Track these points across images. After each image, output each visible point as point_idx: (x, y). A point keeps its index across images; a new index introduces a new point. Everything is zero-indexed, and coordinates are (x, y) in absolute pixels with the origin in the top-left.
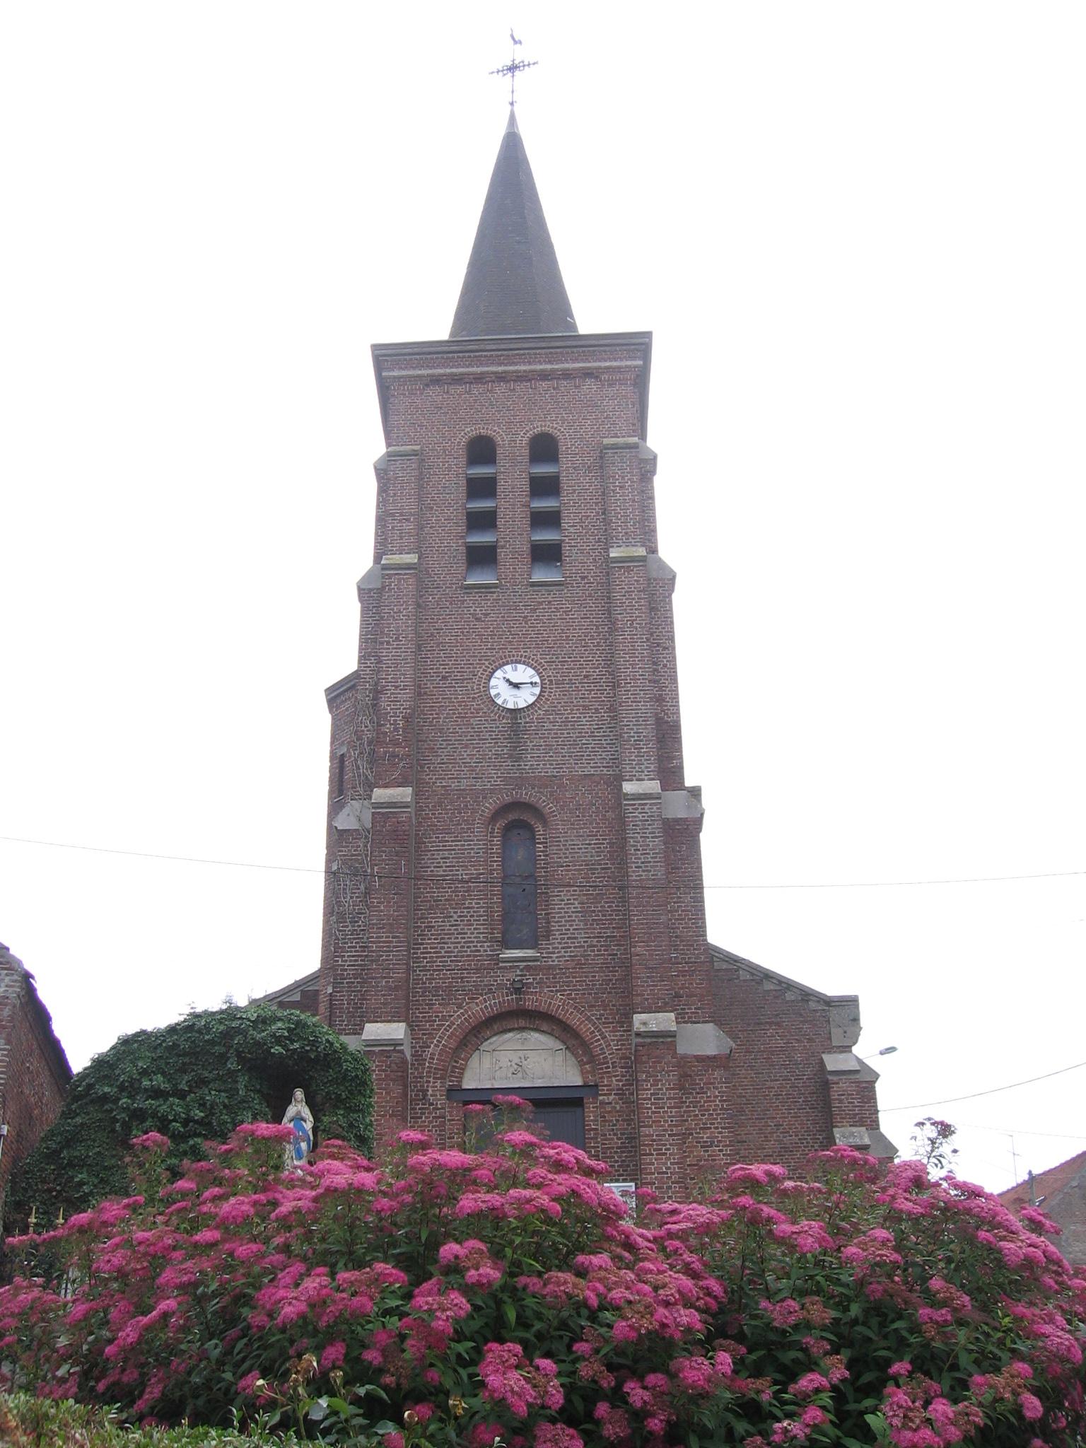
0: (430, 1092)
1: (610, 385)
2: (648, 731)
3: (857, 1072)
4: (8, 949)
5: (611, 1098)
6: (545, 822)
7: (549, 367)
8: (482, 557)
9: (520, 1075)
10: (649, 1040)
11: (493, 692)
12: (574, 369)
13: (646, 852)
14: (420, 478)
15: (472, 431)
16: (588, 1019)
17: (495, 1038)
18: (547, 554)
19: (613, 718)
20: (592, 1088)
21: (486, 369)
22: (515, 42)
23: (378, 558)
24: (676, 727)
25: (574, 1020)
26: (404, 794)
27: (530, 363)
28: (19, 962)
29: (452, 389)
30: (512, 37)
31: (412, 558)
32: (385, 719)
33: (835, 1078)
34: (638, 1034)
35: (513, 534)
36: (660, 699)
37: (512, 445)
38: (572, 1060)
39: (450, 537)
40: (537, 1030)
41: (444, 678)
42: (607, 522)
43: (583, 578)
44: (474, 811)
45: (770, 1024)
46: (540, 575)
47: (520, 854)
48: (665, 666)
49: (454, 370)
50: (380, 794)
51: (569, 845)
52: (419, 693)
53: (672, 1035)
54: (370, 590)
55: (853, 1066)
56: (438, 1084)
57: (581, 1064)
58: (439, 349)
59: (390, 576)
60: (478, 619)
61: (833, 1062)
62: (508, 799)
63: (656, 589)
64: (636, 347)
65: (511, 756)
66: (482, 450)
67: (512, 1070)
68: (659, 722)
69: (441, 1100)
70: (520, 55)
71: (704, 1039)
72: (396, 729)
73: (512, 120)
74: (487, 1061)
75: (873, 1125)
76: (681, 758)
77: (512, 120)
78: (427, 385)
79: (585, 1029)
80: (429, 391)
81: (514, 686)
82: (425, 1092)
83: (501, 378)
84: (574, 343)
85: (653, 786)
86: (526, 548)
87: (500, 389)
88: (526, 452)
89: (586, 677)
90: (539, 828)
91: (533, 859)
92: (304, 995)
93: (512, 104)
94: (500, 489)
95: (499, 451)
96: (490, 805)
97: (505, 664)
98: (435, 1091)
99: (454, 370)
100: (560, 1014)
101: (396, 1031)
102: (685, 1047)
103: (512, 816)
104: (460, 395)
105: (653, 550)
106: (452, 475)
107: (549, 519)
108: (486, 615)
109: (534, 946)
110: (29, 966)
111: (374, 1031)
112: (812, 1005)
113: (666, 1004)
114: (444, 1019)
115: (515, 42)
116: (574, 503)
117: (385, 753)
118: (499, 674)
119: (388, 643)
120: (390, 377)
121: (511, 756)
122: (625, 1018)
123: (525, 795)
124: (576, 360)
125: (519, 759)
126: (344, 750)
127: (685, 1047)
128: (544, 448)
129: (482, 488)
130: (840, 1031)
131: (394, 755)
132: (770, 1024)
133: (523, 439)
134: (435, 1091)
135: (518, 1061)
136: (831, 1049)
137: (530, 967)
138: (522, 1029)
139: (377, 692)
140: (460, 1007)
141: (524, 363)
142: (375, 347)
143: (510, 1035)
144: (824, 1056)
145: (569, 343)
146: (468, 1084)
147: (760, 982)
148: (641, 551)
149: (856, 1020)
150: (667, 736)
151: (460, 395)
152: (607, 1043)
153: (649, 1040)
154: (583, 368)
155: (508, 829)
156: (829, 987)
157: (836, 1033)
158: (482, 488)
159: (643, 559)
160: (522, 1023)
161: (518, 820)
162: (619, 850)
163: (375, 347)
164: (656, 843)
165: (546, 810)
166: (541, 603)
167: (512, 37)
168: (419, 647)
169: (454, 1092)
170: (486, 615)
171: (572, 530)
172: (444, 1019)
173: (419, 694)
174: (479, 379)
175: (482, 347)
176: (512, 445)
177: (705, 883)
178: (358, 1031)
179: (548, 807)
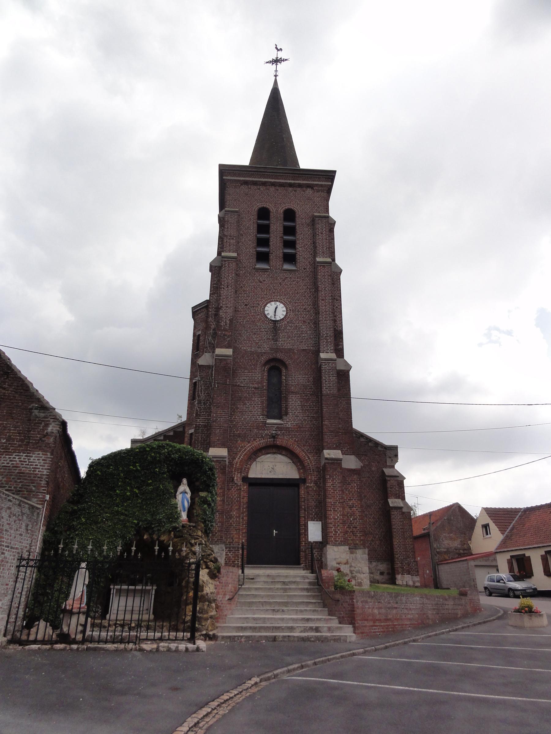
0: (235, 479)
1: (317, 192)
2: (331, 333)
3: (398, 476)
4: (54, 409)
5: (312, 485)
6: (286, 367)
7: (293, 182)
8: (263, 257)
9: (273, 473)
10: (330, 461)
11: (266, 312)
12: (303, 184)
13: (329, 383)
14: (238, 222)
15: (260, 205)
16: (303, 450)
17: (263, 456)
18: (290, 259)
19: (315, 327)
20: (303, 481)
21: (266, 180)
22: (278, 50)
23: (219, 253)
24: (341, 333)
25: (297, 450)
26: (229, 352)
27: (285, 179)
28: (60, 416)
29: (252, 187)
30: (276, 48)
31: (235, 255)
32: (221, 320)
33: (389, 479)
34: (326, 459)
35: (276, 248)
36: (335, 321)
37: (277, 211)
38: (295, 467)
39: (249, 247)
40: (280, 454)
41: (246, 305)
42: (315, 247)
43: (304, 269)
44: (257, 361)
45: (363, 455)
46: (286, 267)
47: (275, 380)
48: (337, 307)
49: (253, 179)
50: (218, 351)
51: (297, 378)
52: (236, 311)
53: (341, 460)
54: (216, 266)
55: (395, 474)
56: (239, 475)
57: (299, 469)
58: (244, 169)
59: (225, 261)
60: (261, 282)
61: (387, 471)
62: (271, 357)
63: (335, 275)
64: (328, 176)
65: (273, 339)
66: (264, 213)
67: (269, 470)
68: (335, 330)
69: (240, 482)
70: (281, 55)
71: (351, 462)
72: (226, 324)
73: (276, 82)
74: (259, 465)
75: (403, 498)
76: (343, 345)
77: (276, 82)
78: (242, 184)
79: (302, 455)
80: (242, 187)
81: (275, 310)
82: (233, 478)
83: (273, 184)
84: (298, 172)
85: (333, 356)
86: (281, 255)
87: (272, 189)
88: (282, 216)
89: (305, 309)
90: (284, 370)
91: (280, 382)
92: (176, 434)
93: (276, 76)
94: (271, 230)
95: (271, 214)
96: (263, 359)
97: (271, 301)
98: (237, 478)
99: (253, 179)
100: (291, 447)
101: (223, 452)
102: (345, 465)
103: (272, 364)
104: (255, 190)
105: (334, 260)
106: (250, 223)
107: (291, 244)
108: (264, 281)
109: (280, 418)
110: (65, 417)
111: (214, 452)
112: (380, 448)
113: (337, 446)
114: (242, 447)
115: (278, 50)
116: (302, 237)
117: (221, 334)
118: (278, 303)
119: (224, 288)
120: (227, 179)
121: (273, 339)
122: (319, 451)
123: (279, 356)
124: (304, 180)
125: (276, 341)
126: (200, 332)
127: (345, 465)
128: (290, 215)
129: (263, 229)
130: (390, 459)
131: (225, 335)
132: (363, 455)
133: (281, 210)
134: (237, 478)
135: (272, 466)
136: (386, 466)
137: (279, 428)
138: (274, 453)
139: (218, 309)
140: (249, 442)
141: (283, 179)
142: (221, 166)
143: (269, 455)
144: (384, 469)
145: (297, 172)
146: (251, 475)
147: (359, 438)
148: (329, 260)
149: (396, 456)
150: (338, 335)
151: (255, 190)
152: (310, 460)
153: (330, 461)
154: (307, 184)
155: (270, 370)
156: (387, 441)
157: (388, 460)
158: (263, 229)
159: (330, 263)
160: (274, 451)
161: (276, 366)
162: (318, 380)
163: (221, 166)
164: (334, 379)
165: (287, 363)
166: (287, 278)
167: (276, 48)
168: (236, 292)
169: (246, 479)
170: (264, 281)
171: (300, 249)
172: (242, 447)
173: (235, 311)
174: (264, 184)
175: (265, 170)
176: (277, 211)
177: (352, 395)
178: (207, 450)
179: (288, 362)
